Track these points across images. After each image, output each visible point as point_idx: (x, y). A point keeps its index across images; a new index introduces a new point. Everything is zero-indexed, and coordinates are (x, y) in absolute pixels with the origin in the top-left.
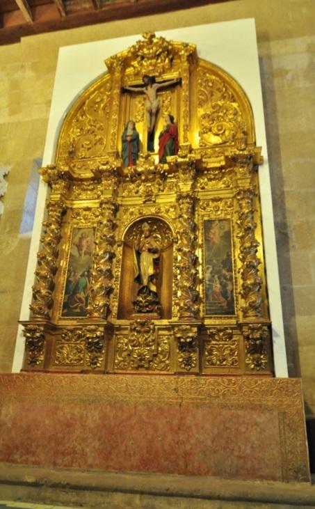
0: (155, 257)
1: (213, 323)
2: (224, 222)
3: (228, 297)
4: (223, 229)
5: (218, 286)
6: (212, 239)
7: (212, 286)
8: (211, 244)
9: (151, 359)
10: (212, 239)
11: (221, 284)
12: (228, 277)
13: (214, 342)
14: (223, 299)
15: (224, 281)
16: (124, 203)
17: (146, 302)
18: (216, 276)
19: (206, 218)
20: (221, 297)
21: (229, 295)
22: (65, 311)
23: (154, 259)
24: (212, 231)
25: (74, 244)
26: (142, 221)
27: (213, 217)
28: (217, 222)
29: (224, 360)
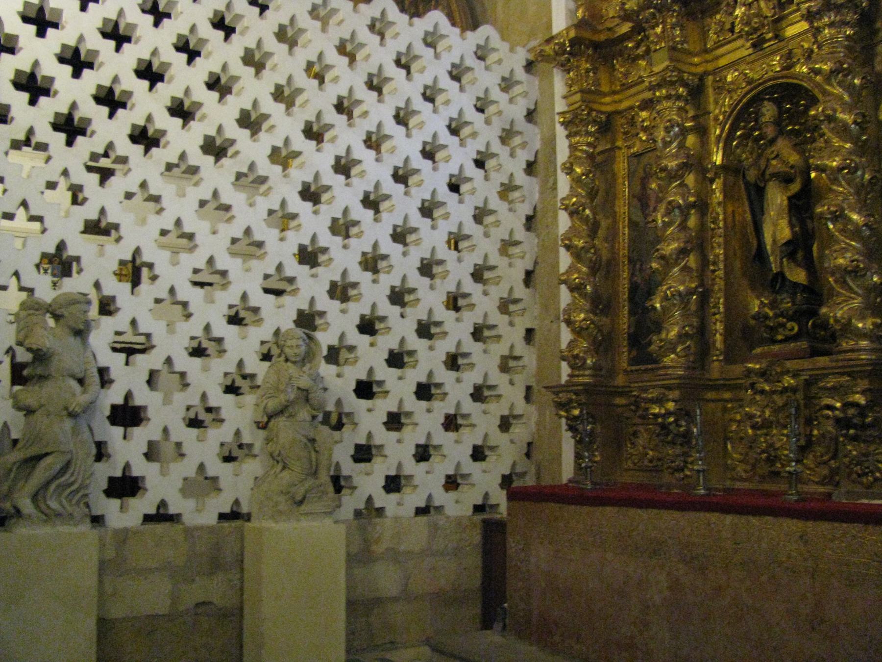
0: (789, 194)
17: (776, 316)
22: (634, 353)
26: (756, 100)
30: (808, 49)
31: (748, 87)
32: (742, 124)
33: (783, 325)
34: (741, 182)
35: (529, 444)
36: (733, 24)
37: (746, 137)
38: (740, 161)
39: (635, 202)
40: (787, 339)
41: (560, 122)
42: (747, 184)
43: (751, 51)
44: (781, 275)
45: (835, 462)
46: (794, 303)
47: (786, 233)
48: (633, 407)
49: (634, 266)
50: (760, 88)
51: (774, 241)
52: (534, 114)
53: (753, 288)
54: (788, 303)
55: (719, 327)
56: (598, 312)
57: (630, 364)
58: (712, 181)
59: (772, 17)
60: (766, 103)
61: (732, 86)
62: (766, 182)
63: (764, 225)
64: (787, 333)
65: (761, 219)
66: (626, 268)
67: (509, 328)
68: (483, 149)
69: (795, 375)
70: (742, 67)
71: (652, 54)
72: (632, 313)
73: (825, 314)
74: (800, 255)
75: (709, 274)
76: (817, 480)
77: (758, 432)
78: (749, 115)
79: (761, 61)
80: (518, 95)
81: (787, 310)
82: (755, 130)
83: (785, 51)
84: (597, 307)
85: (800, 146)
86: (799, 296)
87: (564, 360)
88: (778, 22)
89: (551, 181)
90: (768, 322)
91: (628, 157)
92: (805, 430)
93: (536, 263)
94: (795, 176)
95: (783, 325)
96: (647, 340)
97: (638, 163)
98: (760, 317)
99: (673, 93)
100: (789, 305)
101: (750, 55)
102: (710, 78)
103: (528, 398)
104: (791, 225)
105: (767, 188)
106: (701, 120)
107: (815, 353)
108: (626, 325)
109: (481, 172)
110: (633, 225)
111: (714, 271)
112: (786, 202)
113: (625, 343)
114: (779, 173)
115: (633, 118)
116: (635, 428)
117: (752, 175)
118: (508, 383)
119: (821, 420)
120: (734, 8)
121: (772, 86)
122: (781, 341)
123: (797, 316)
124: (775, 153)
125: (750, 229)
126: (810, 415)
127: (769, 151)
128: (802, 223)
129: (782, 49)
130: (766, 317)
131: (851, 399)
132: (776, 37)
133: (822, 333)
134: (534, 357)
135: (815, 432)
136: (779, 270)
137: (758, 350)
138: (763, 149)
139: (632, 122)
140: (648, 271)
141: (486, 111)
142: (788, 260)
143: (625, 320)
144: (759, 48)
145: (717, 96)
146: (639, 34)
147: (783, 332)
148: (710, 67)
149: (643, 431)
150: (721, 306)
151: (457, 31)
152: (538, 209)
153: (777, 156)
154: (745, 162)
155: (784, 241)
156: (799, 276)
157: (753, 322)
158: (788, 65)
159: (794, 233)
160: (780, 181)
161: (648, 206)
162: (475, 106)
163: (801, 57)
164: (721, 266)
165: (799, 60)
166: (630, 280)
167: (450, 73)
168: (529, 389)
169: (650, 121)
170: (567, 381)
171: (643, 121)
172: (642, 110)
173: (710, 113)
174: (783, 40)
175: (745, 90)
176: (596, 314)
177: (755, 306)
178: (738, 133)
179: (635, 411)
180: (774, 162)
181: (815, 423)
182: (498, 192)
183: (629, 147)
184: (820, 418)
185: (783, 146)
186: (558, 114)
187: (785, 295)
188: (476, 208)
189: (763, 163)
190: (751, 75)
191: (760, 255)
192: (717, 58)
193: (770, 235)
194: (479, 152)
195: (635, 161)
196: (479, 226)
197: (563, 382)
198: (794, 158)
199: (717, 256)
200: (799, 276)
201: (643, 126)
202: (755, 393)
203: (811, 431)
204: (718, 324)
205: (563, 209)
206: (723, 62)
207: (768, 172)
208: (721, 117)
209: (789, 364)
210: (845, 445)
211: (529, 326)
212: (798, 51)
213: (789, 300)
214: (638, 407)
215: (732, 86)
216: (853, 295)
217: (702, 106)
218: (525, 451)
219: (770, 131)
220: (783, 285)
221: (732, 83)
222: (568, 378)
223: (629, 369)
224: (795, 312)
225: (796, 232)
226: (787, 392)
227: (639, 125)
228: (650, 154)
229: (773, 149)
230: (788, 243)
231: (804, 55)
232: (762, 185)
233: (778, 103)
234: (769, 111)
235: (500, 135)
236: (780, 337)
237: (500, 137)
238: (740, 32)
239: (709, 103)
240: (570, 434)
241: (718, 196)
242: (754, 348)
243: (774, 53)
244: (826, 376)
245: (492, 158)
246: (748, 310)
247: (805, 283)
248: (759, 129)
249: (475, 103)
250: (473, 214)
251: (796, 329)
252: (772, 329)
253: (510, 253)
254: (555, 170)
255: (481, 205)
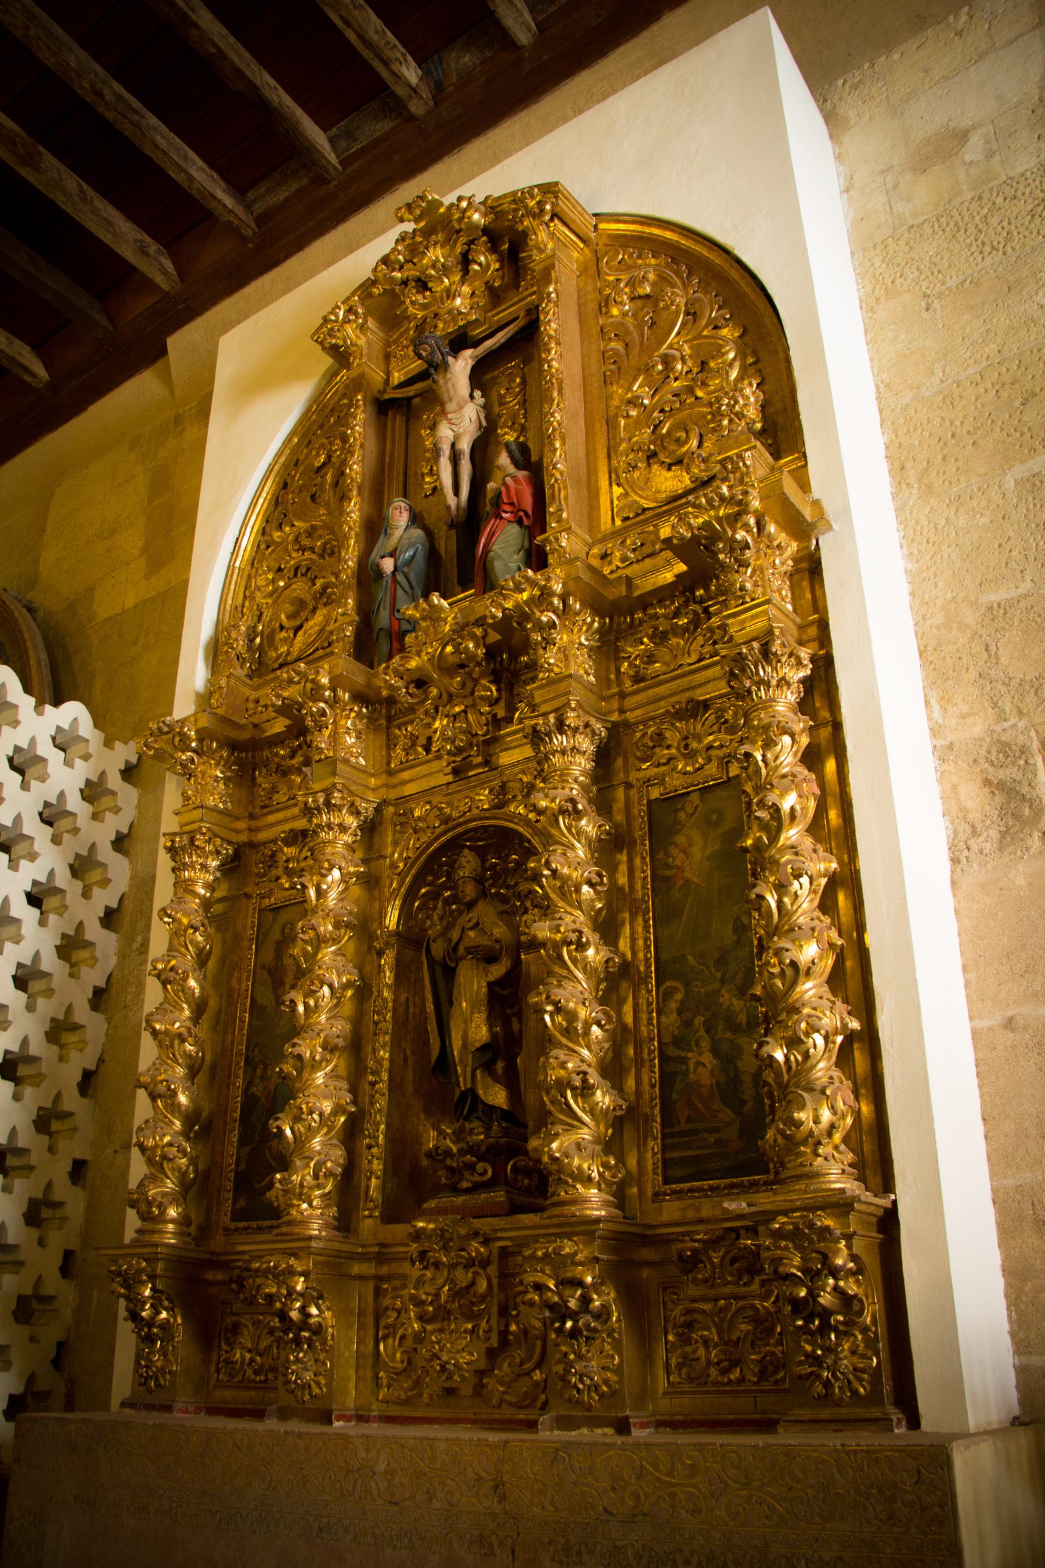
0: (491, 978)
1: (690, 1214)
2: (721, 793)
3: (743, 1103)
4: (718, 823)
5: (707, 1058)
6: (681, 869)
7: (684, 1061)
8: (676, 894)
9: (482, 1365)
10: (681, 869)
11: (715, 1051)
12: (742, 1018)
13: (692, 1291)
14: (727, 1114)
15: (729, 1035)
16: (262, 836)
17: (462, 1152)
18: (699, 1020)
19: (655, 793)
20: (717, 1105)
21: (748, 1092)
22: (242, 1203)
23: (490, 985)
24: (681, 839)
25: (263, 967)
26: (453, 847)
27: (675, 782)
28: (695, 798)
29: (734, 1363)
30: (528, 783)
31: (443, 827)
32: (430, 878)
33: (471, 1167)
34: (424, 958)
35: (61, 1346)
36: (429, 739)
37: (434, 896)
38: (424, 930)
39: (265, 975)
40: (476, 1188)
41: (165, 848)
42: (431, 961)
43: (450, 778)
44: (471, 1094)
45: (541, 1373)
46: (487, 1136)
47: (480, 1032)
48: (234, 1286)
49: (254, 1070)
50: (460, 830)
51: (465, 1045)
52: (127, 841)
53: (428, 1111)
54: (479, 1134)
55: (377, 1166)
56: (192, 1135)
57: (234, 1219)
58: (380, 953)
59: (484, 736)
60: (466, 851)
61: (421, 824)
62: (457, 962)
63: (451, 1022)
64: (477, 1178)
65: (449, 1011)
66: (241, 1072)
67: (48, 1155)
68: (43, 879)
69: (486, 1242)
70: (436, 799)
71: (314, 765)
72: (243, 1141)
73: (535, 1150)
74: (500, 1066)
75: (367, 1087)
76: (514, 1400)
77: (429, 1327)
78: (441, 866)
79: (464, 793)
80: (106, 809)
81: (478, 1144)
82: (447, 889)
83: (497, 783)
84: (191, 1128)
85: (509, 915)
86: (495, 1127)
87: (132, 1207)
88: (491, 744)
89: (139, 939)
90: (449, 1162)
91: (260, 910)
92: (498, 1323)
93: (101, 1060)
94: (500, 956)
95: (471, 1167)
96: (265, 1182)
97: (274, 919)
98: (438, 1155)
99: (337, 821)
100: (482, 1137)
101: (449, 784)
102: (391, 809)
103: (66, 1270)
104: (490, 1021)
105: (458, 970)
106: (372, 865)
107: (515, 1209)
108: (234, 1158)
109: (36, 912)
110: (256, 1008)
111: (373, 1084)
112: (484, 990)
113: (230, 1185)
114: (479, 946)
115: (274, 855)
116: (235, 1318)
117: (438, 949)
118: (36, 1242)
119: (522, 1307)
120: (434, 719)
121: (475, 829)
122: (467, 1191)
123: (491, 1154)
124: (474, 921)
125: (432, 1027)
126: (507, 1301)
127: (465, 917)
128: (507, 1025)
129: (492, 781)
130: (448, 1153)
131: (569, 1275)
132: (486, 763)
133: (526, 1181)
134: (82, 1205)
135: (513, 1327)
136: (469, 1086)
137: (432, 1203)
138: (455, 917)
139: (272, 860)
140: (275, 1079)
141: (55, 825)
142: (482, 1072)
143: (233, 1150)
144: (462, 776)
145: (398, 835)
146: (297, 738)
147: (472, 1178)
148: (392, 795)
149: (249, 1324)
150: (381, 1137)
151: (31, 701)
152: (114, 979)
153: (477, 924)
154: (430, 932)
155: (478, 1045)
156: (498, 1096)
157: (425, 1162)
158: (502, 798)
159: (493, 1035)
160: (477, 960)
161: (282, 983)
162: (41, 814)
163: (518, 793)
164: (385, 1077)
165: (514, 796)
166: (246, 1091)
167: (10, 760)
168: (68, 1255)
169: (298, 862)
170: (133, 1241)
171: (287, 861)
172: (288, 844)
173: (385, 857)
174: (496, 768)
175: (438, 831)
176: (188, 1138)
177: (431, 1140)
178: (423, 891)
179: (238, 1292)
180: (472, 934)
181: (514, 1313)
182: (57, 947)
183: (262, 897)
184: (522, 1306)
185: (485, 912)
186: (164, 835)
187: (476, 1124)
188: (20, 965)
189: (455, 935)
190: (447, 810)
191: (444, 1063)
192: (404, 783)
193: (459, 1036)
194: (35, 883)
195: (271, 915)
196: (19, 993)
197: (127, 1241)
198: (500, 931)
199: (379, 1062)
200: (498, 1096)
201: (287, 867)
202: (426, 1268)
203: (507, 1326)
204: (376, 1162)
205: (154, 976)
206: (409, 789)
207: (461, 948)
208: (401, 865)
209: (477, 1223)
210: (558, 1345)
211: (79, 1156)
212: (514, 786)
213: (481, 1130)
214: (242, 1286)
215: (421, 824)
216: (576, 1123)
217: (376, 847)
218: (53, 1355)
219: (469, 891)
220: (473, 1109)
221: (420, 819)
222: (136, 1235)
223: (232, 1226)
224: (490, 1148)
225: (497, 1033)
226: (474, 1265)
227: (281, 863)
228: (294, 908)
229: (470, 915)
230: (484, 1048)
231: (522, 791)
232: (453, 965)
233: (481, 853)
234: (468, 864)
235: (72, 862)
236: (465, 1185)
237: (71, 866)
238: (439, 750)
239: (386, 844)
240: (130, 1325)
241: (388, 976)
242: (426, 1201)
243: (481, 785)
244: (535, 1239)
245: (55, 895)
246: (421, 1145)
247: (505, 1107)
248: (454, 888)
249: (41, 810)
250: (13, 973)
251: (490, 1173)
252: (451, 1170)
253: (63, 1041)
254: (150, 918)
255: (28, 961)
